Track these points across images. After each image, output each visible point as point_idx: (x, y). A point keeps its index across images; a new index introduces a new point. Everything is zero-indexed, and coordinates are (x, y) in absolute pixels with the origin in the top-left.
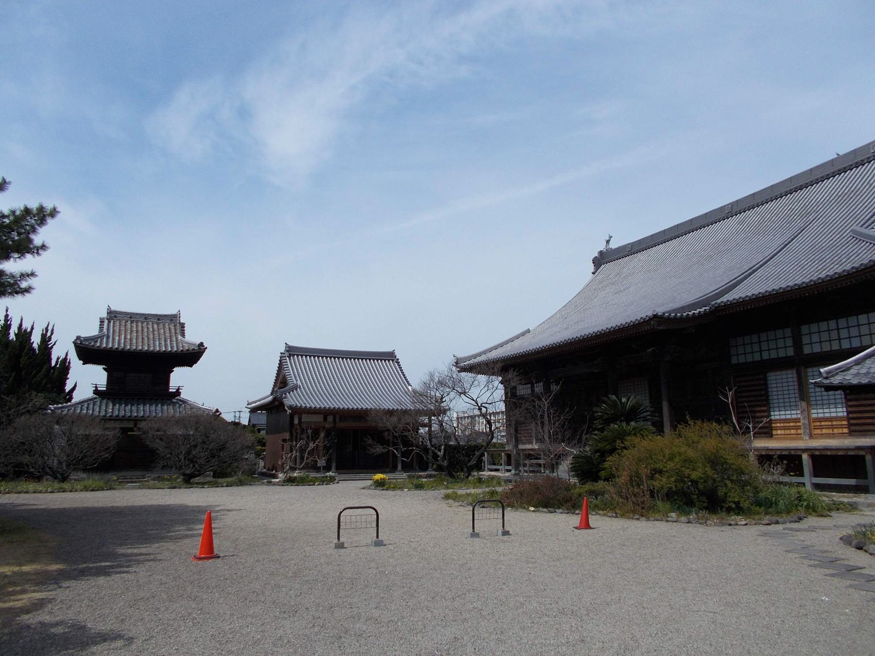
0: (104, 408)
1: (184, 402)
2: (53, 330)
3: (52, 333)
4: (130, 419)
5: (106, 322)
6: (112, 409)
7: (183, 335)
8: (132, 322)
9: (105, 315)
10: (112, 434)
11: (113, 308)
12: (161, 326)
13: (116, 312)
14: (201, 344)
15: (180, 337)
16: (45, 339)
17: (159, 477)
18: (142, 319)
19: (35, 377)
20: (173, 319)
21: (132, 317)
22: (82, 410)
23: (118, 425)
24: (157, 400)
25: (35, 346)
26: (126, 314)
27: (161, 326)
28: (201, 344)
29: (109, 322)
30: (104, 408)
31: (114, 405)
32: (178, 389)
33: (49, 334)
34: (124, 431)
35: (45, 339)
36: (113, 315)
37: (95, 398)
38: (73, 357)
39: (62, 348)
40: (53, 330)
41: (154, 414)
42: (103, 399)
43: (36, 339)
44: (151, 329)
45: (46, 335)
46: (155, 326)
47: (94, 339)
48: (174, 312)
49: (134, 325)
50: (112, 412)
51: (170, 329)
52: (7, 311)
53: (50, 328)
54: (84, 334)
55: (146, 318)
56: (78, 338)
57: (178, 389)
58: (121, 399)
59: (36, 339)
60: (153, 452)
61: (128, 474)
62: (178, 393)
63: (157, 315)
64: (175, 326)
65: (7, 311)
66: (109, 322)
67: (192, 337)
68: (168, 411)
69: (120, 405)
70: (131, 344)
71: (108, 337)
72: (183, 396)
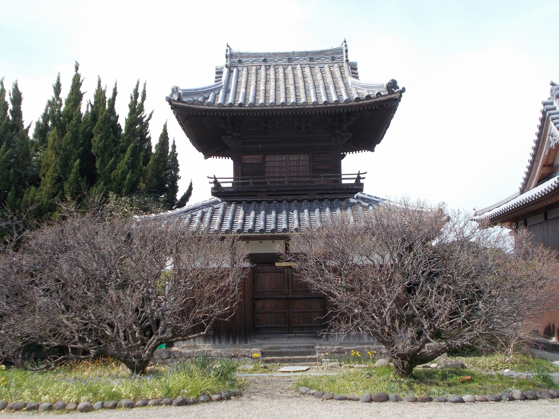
0: (229, 217)
1: (371, 201)
2: (144, 91)
3: (144, 99)
4: (274, 237)
5: (225, 71)
6: (242, 219)
7: (355, 75)
8: (267, 69)
9: (222, 62)
10: (227, 263)
11: (235, 50)
12: (317, 69)
13: (241, 55)
14: (392, 85)
15: (350, 80)
16: (136, 109)
17: (340, 352)
18: (284, 61)
19: (113, 169)
20: (336, 55)
21: (266, 60)
22: (191, 221)
23: (244, 249)
24: (321, 200)
25: (122, 122)
26: (256, 56)
27: (317, 69)
28: (392, 85)
29: (231, 72)
30: (229, 217)
31: (246, 213)
32: (358, 178)
33: (139, 100)
34: (262, 262)
35: (136, 109)
36: (235, 60)
37: (216, 202)
38: (180, 139)
39: (161, 122)
40: (144, 91)
41: (319, 224)
42: (230, 203)
43: (122, 113)
44: (300, 75)
45: (136, 102)
46: (307, 70)
47: (205, 92)
48: (337, 44)
49: (272, 72)
50: (243, 224)
51: (332, 73)
52: (77, 68)
53: (140, 91)
54: (186, 85)
55: (290, 60)
56: (175, 90)
57: (358, 178)
58: (259, 202)
59: (122, 113)
60: (323, 301)
61: (284, 343)
62: (358, 187)
63: (307, 53)
64: (340, 67)
65: (77, 68)
66: (231, 72)
67: (370, 80)
68: (347, 217)
69: (257, 213)
70: (266, 97)
71: (227, 91)
72: (369, 190)
